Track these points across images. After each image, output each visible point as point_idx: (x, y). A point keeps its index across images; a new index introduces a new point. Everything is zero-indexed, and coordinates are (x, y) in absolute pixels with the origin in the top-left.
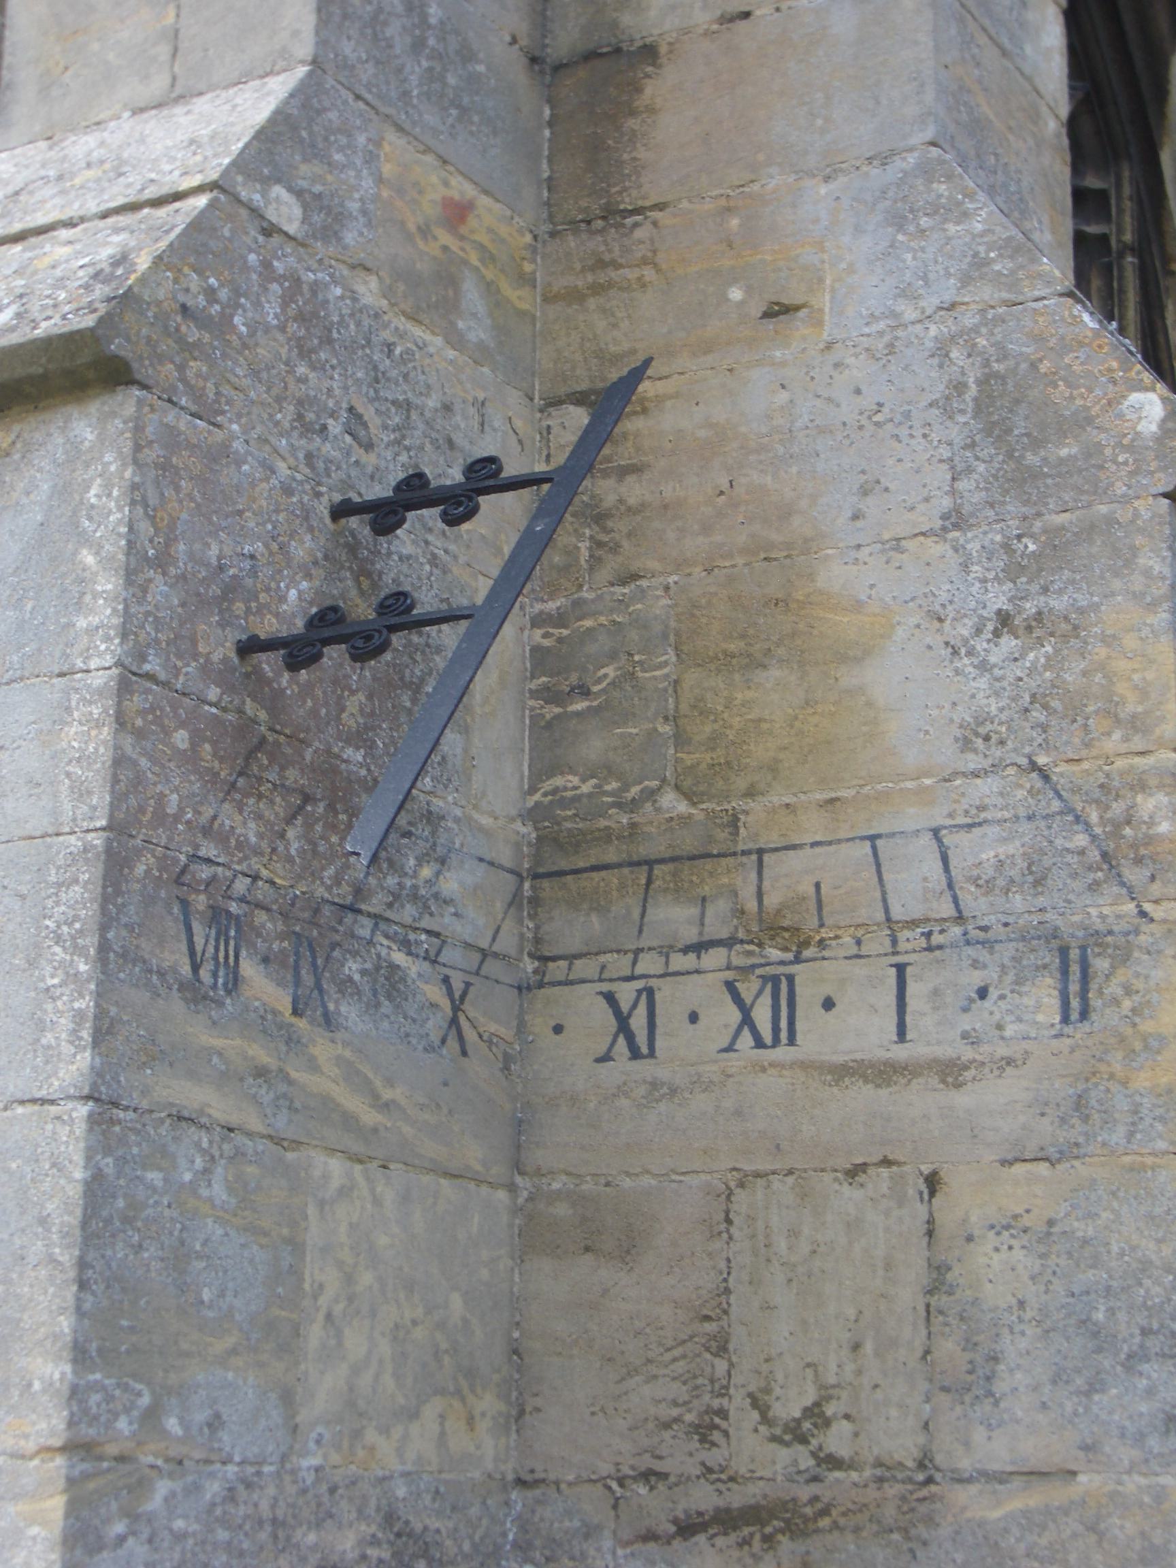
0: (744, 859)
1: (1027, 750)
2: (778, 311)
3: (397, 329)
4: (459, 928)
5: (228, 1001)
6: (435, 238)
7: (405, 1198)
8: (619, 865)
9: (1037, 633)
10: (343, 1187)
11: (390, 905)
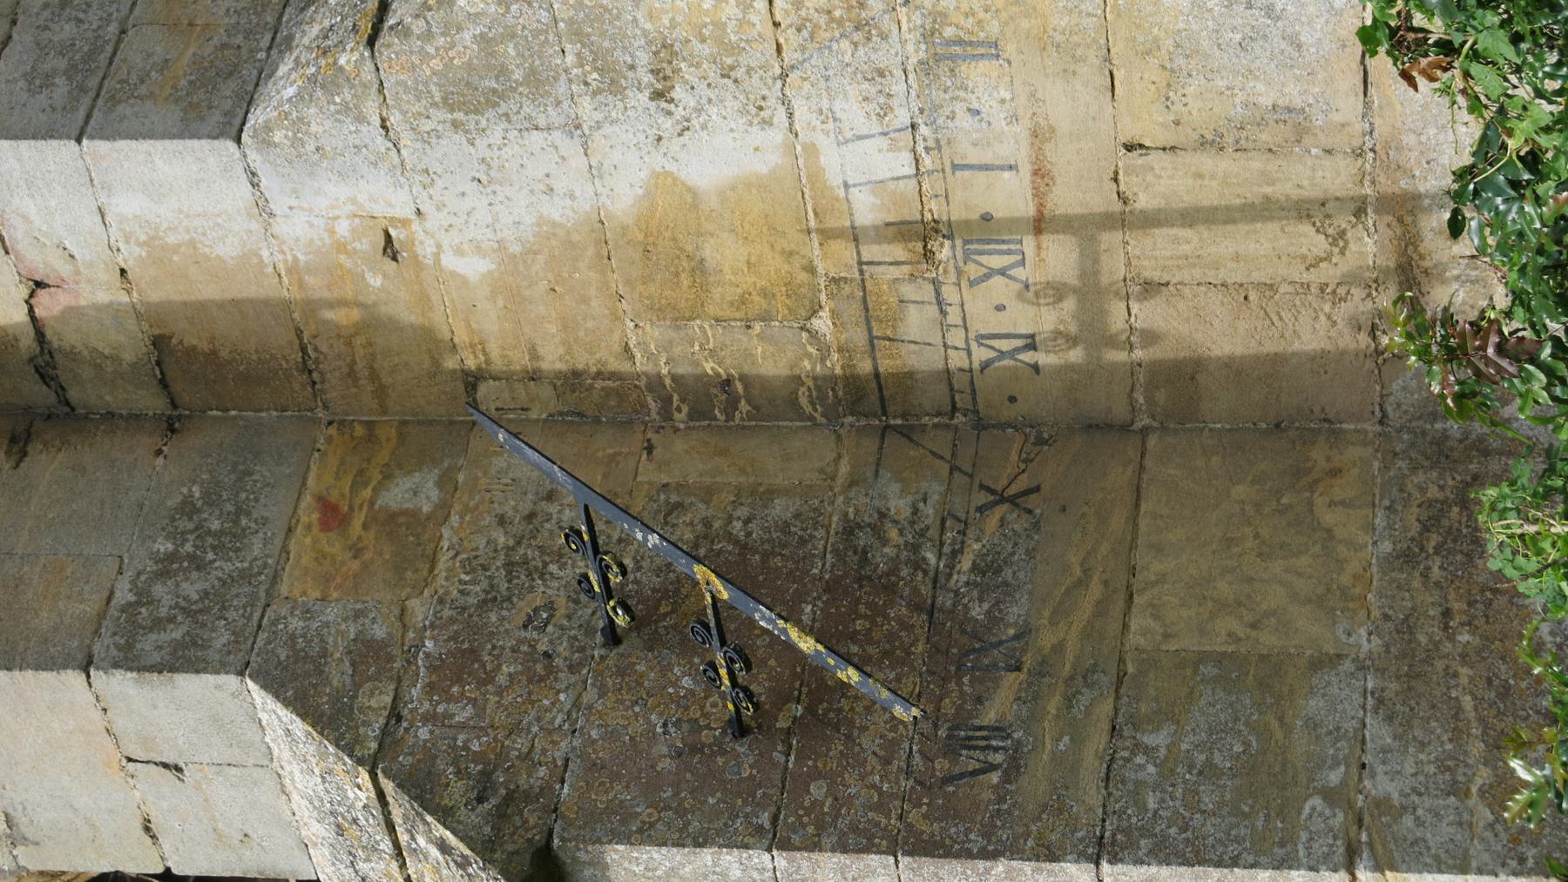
0: (867, 276)
1: (770, 81)
2: (389, 248)
3: (447, 579)
4: (936, 497)
5: (1015, 736)
6: (359, 538)
7: (1158, 549)
8: (874, 359)
9: (669, 72)
10: (1152, 615)
11: (925, 572)
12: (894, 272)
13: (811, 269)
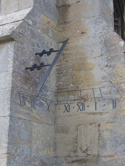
2: (83, 33)
7: (43, 127)
8: (66, 92)
12: (79, 94)
13: (80, 84)
